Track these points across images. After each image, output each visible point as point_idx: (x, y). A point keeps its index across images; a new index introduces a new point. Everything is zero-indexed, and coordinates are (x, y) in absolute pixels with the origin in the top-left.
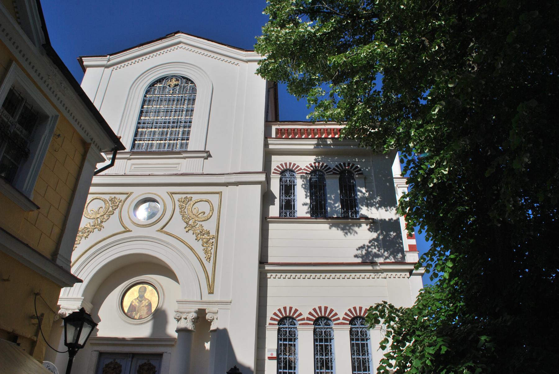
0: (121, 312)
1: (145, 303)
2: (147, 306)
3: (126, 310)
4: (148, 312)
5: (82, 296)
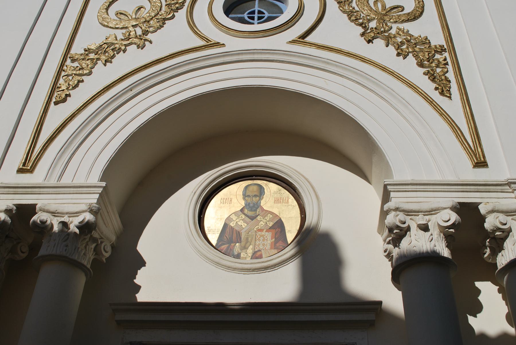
1: (263, 222)
4: (276, 242)
5: (101, 180)
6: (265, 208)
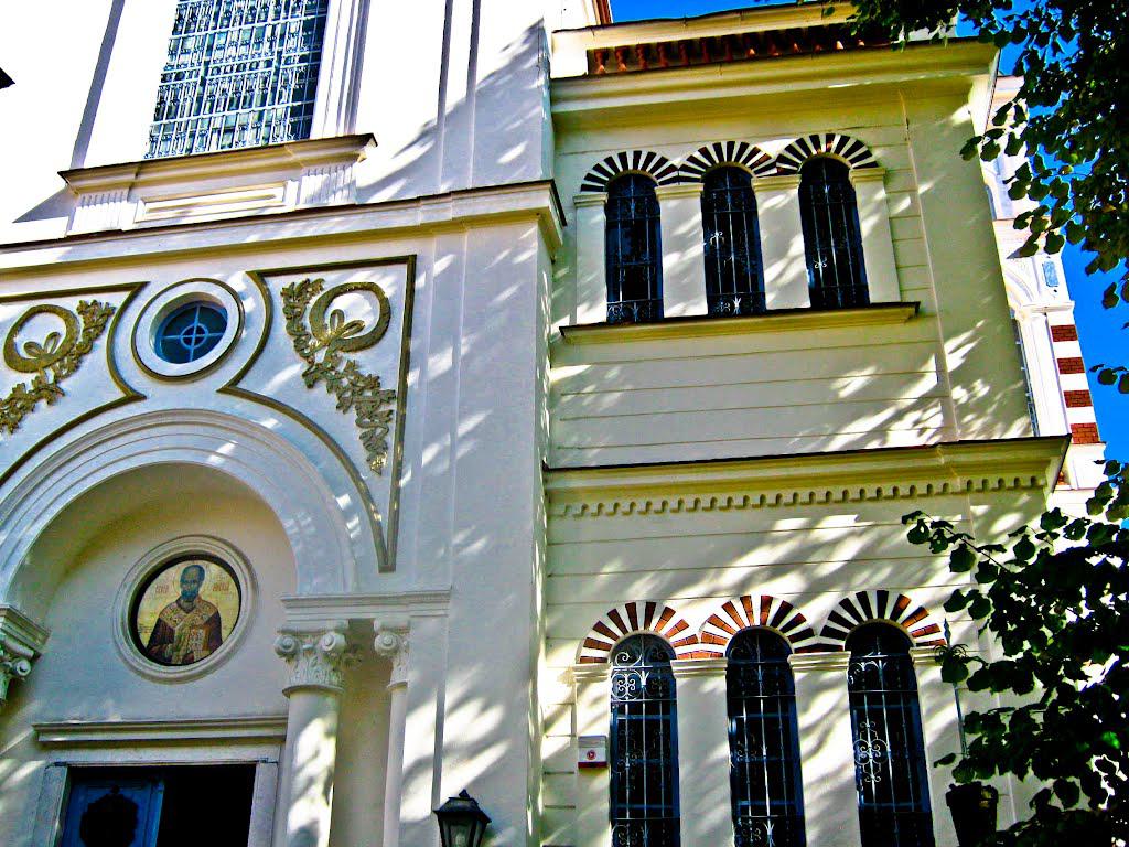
1: (199, 618)
3: (145, 638)
6: (203, 598)
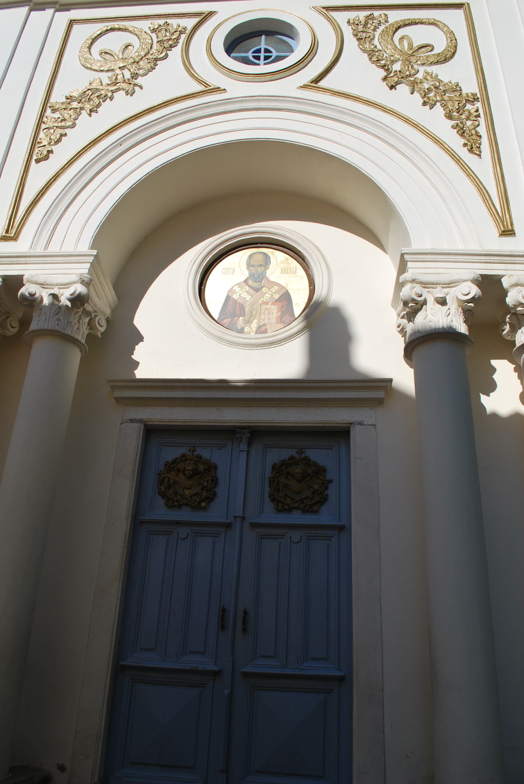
0: (204, 315)
1: (268, 294)
2: (277, 301)
4: (282, 316)
5: (92, 248)
